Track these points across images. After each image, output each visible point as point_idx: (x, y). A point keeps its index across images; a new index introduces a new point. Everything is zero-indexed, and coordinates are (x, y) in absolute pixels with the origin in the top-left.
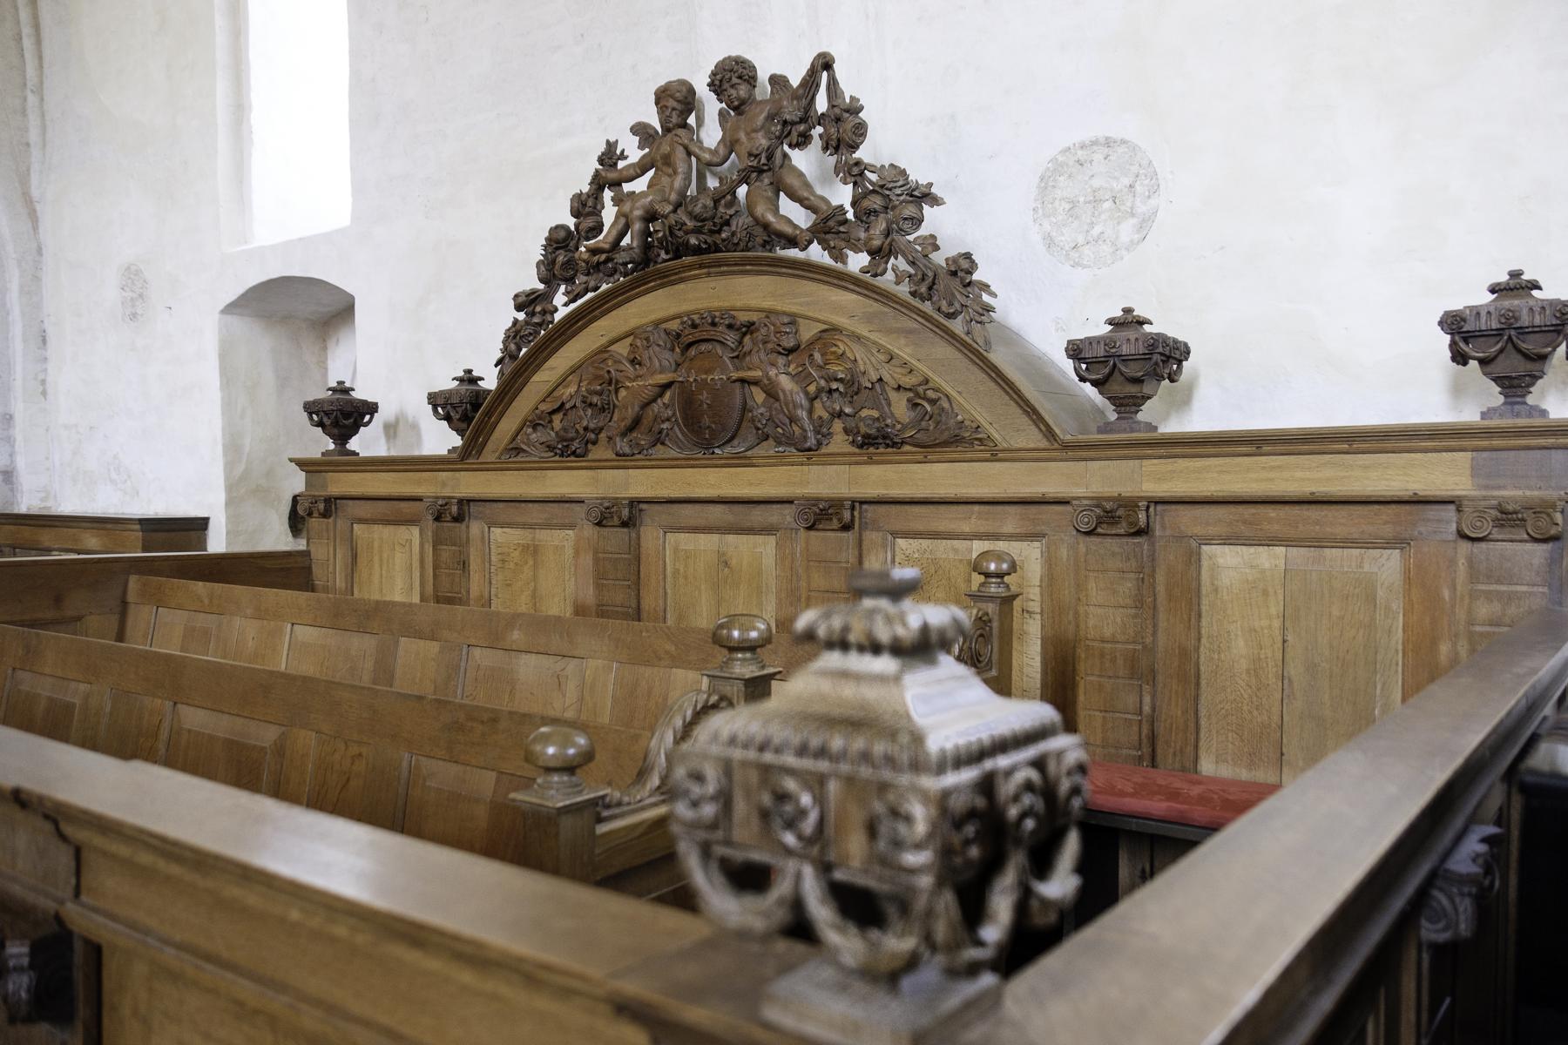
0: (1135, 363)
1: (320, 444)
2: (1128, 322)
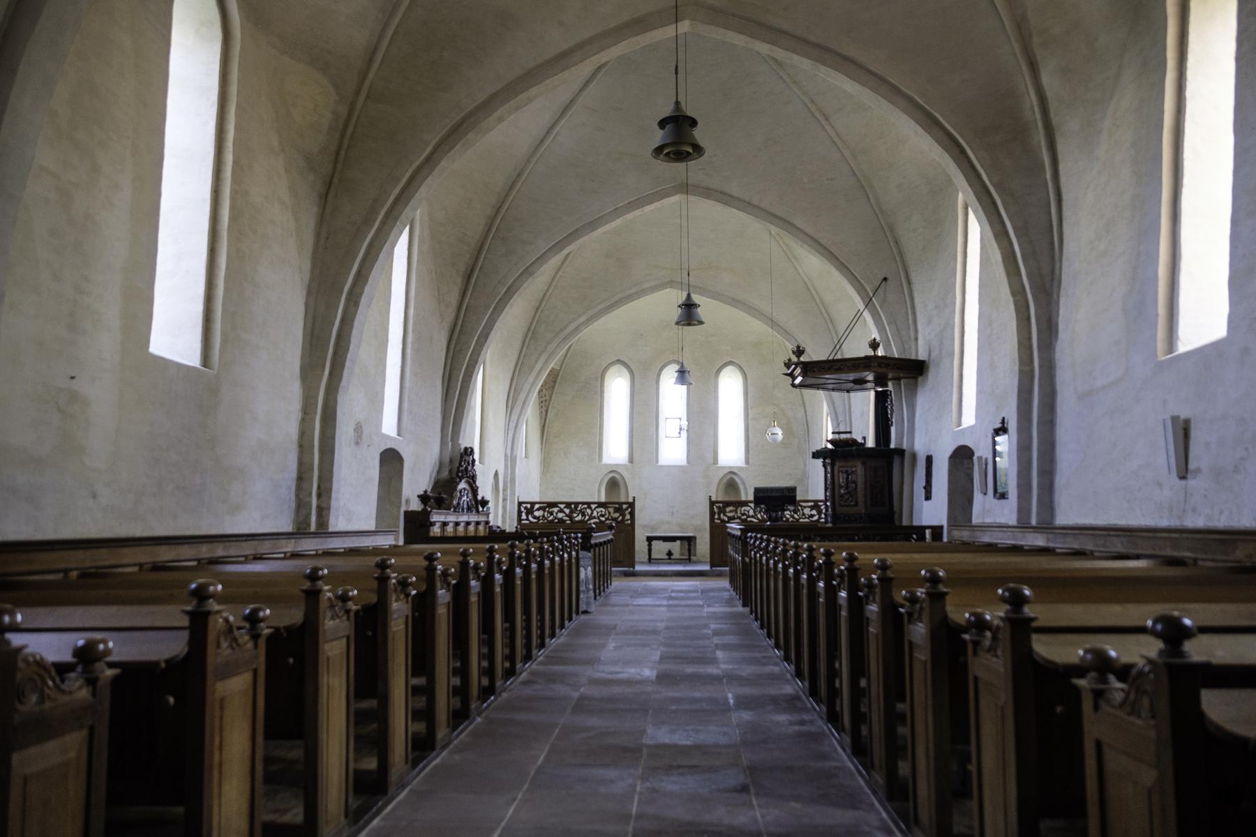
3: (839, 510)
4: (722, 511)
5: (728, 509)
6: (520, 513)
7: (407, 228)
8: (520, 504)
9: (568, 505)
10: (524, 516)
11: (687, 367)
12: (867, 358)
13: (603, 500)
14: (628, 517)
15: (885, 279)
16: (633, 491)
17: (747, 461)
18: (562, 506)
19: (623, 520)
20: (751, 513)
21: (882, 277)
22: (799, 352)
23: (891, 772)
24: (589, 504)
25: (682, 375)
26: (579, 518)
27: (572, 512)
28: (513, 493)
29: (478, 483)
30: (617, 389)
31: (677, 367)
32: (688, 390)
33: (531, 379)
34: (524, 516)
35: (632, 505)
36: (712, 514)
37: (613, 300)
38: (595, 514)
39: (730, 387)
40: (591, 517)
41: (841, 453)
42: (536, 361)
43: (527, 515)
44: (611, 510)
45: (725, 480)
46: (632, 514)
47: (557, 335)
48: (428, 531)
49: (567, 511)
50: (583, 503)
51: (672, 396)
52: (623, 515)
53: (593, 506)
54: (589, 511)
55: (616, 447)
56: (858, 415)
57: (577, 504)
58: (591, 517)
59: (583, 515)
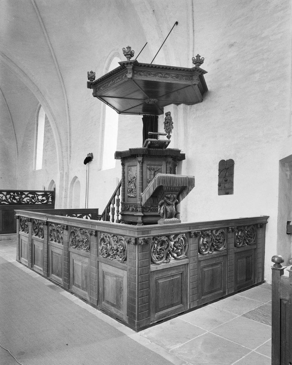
15: (177, 23)
20: (4, 198)
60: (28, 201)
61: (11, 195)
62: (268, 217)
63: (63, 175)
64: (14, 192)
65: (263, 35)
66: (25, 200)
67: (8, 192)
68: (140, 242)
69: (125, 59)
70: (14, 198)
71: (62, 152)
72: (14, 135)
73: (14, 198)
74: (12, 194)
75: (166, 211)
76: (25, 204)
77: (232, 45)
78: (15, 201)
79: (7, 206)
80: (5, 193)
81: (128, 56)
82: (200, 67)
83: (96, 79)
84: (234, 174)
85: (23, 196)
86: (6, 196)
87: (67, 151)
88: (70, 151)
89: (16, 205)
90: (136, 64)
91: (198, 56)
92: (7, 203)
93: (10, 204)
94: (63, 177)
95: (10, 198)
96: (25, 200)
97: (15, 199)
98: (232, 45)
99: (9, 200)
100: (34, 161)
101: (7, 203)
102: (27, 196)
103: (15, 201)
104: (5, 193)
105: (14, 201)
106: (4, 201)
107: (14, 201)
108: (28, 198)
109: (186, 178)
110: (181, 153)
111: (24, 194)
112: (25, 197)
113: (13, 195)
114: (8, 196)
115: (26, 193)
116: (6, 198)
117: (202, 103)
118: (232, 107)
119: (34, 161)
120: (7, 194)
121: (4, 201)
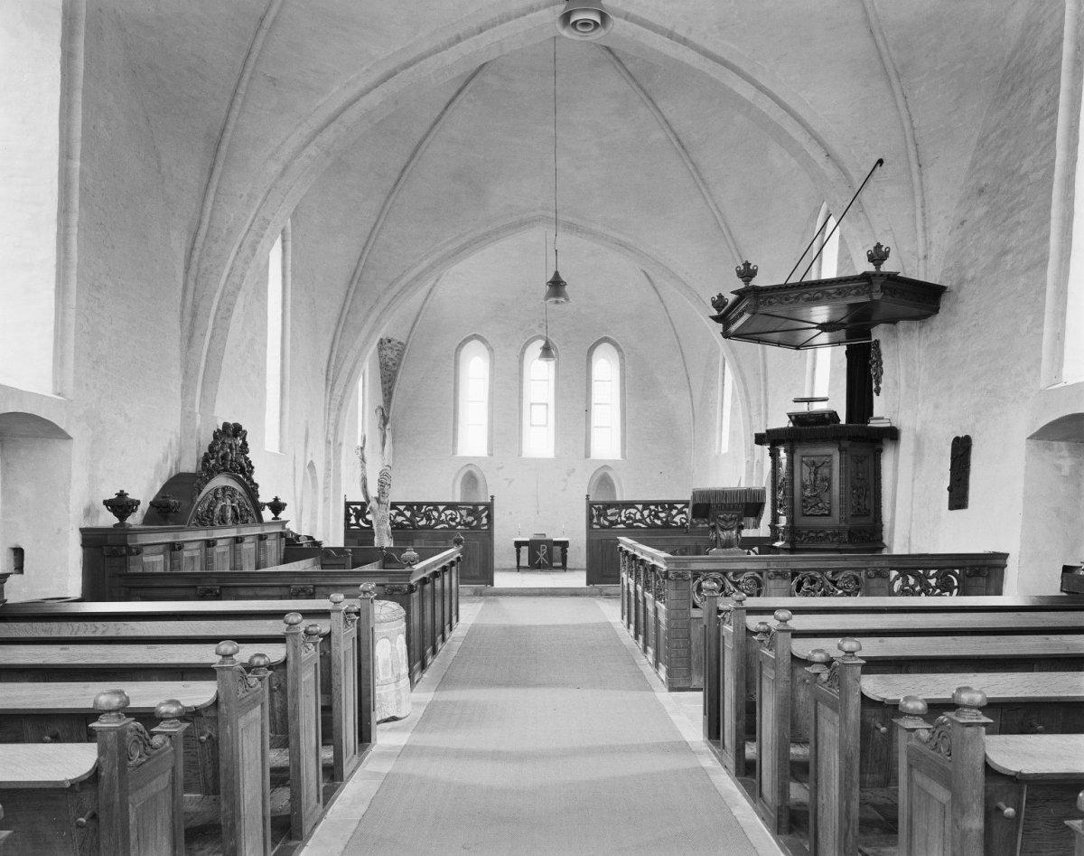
0: (277, 507)
1: (108, 519)
2: (122, 495)
3: (802, 521)
4: (602, 513)
5: (609, 512)
6: (348, 516)
7: (278, 242)
8: (348, 505)
9: (409, 506)
10: (353, 521)
11: (553, 340)
12: (866, 277)
13: (458, 499)
14: (484, 521)
15: (880, 162)
16: (494, 487)
17: (623, 455)
18: (402, 508)
19: (478, 527)
20: (638, 516)
21: (876, 159)
22: (747, 273)
23: (740, 751)
24: (435, 505)
25: (547, 351)
26: (424, 522)
27: (414, 515)
28: (337, 490)
29: (256, 478)
30: (476, 369)
31: (541, 343)
32: (557, 366)
33: (358, 344)
34: (353, 521)
35: (489, 507)
36: (590, 518)
37: (463, 241)
38: (443, 517)
39: (606, 368)
40: (439, 522)
41: (808, 430)
42: (365, 321)
43: (357, 520)
44: (464, 513)
45: (600, 473)
46: (490, 517)
47: (392, 284)
48: (126, 565)
49: (408, 514)
50: (428, 504)
51: (540, 375)
52: (478, 519)
53: (441, 508)
54: (435, 514)
55: (473, 440)
56: (821, 376)
57: (420, 505)
58: (439, 522)
59: (429, 519)
60: (684, 521)
61: (650, 509)
62: (1007, 555)
63: (752, 467)
64: (656, 504)
65: (1022, 171)
66: (677, 519)
67: (646, 505)
68: (670, 576)
69: (741, 285)
70: (657, 516)
71: (750, 417)
72: (686, 379)
73: (657, 516)
74: (652, 507)
75: (718, 538)
76: (677, 527)
77: (981, 191)
78: (658, 522)
79: (643, 530)
80: (640, 507)
81: (745, 278)
82: (882, 270)
83: (729, 303)
84: (971, 467)
85: (674, 512)
86: (641, 513)
87: (760, 414)
88: (766, 414)
89: (660, 530)
90: (759, 291)
91: (879, 246)
92: (644, 526)
93: (649, 527)
94: (752, 471)
95: (649, 516)
96: (677, 519)
97: (659, 518)
98: (981, 191)
99: (648, 520)
100: (717, 434)
101: (644, 526)
102: (681, 512)
103: (658, 522)
104: (640, 507)
105: (656, 521)
106: (639, 521)
107: (656, 521)
108: (684, 516)
109: (746, 491)
110: (323, 546)
111: (676, 508)
112: (678, 514)
113: (654, 510)
114: (646, 513)
115: (679, 506)
116: (642, 515)
117: (938, 317)
118: (975, 326)
119: (717, 434)
120: (644, 509)
121: (639, 521)
